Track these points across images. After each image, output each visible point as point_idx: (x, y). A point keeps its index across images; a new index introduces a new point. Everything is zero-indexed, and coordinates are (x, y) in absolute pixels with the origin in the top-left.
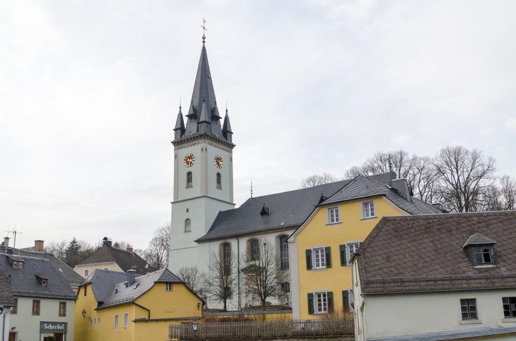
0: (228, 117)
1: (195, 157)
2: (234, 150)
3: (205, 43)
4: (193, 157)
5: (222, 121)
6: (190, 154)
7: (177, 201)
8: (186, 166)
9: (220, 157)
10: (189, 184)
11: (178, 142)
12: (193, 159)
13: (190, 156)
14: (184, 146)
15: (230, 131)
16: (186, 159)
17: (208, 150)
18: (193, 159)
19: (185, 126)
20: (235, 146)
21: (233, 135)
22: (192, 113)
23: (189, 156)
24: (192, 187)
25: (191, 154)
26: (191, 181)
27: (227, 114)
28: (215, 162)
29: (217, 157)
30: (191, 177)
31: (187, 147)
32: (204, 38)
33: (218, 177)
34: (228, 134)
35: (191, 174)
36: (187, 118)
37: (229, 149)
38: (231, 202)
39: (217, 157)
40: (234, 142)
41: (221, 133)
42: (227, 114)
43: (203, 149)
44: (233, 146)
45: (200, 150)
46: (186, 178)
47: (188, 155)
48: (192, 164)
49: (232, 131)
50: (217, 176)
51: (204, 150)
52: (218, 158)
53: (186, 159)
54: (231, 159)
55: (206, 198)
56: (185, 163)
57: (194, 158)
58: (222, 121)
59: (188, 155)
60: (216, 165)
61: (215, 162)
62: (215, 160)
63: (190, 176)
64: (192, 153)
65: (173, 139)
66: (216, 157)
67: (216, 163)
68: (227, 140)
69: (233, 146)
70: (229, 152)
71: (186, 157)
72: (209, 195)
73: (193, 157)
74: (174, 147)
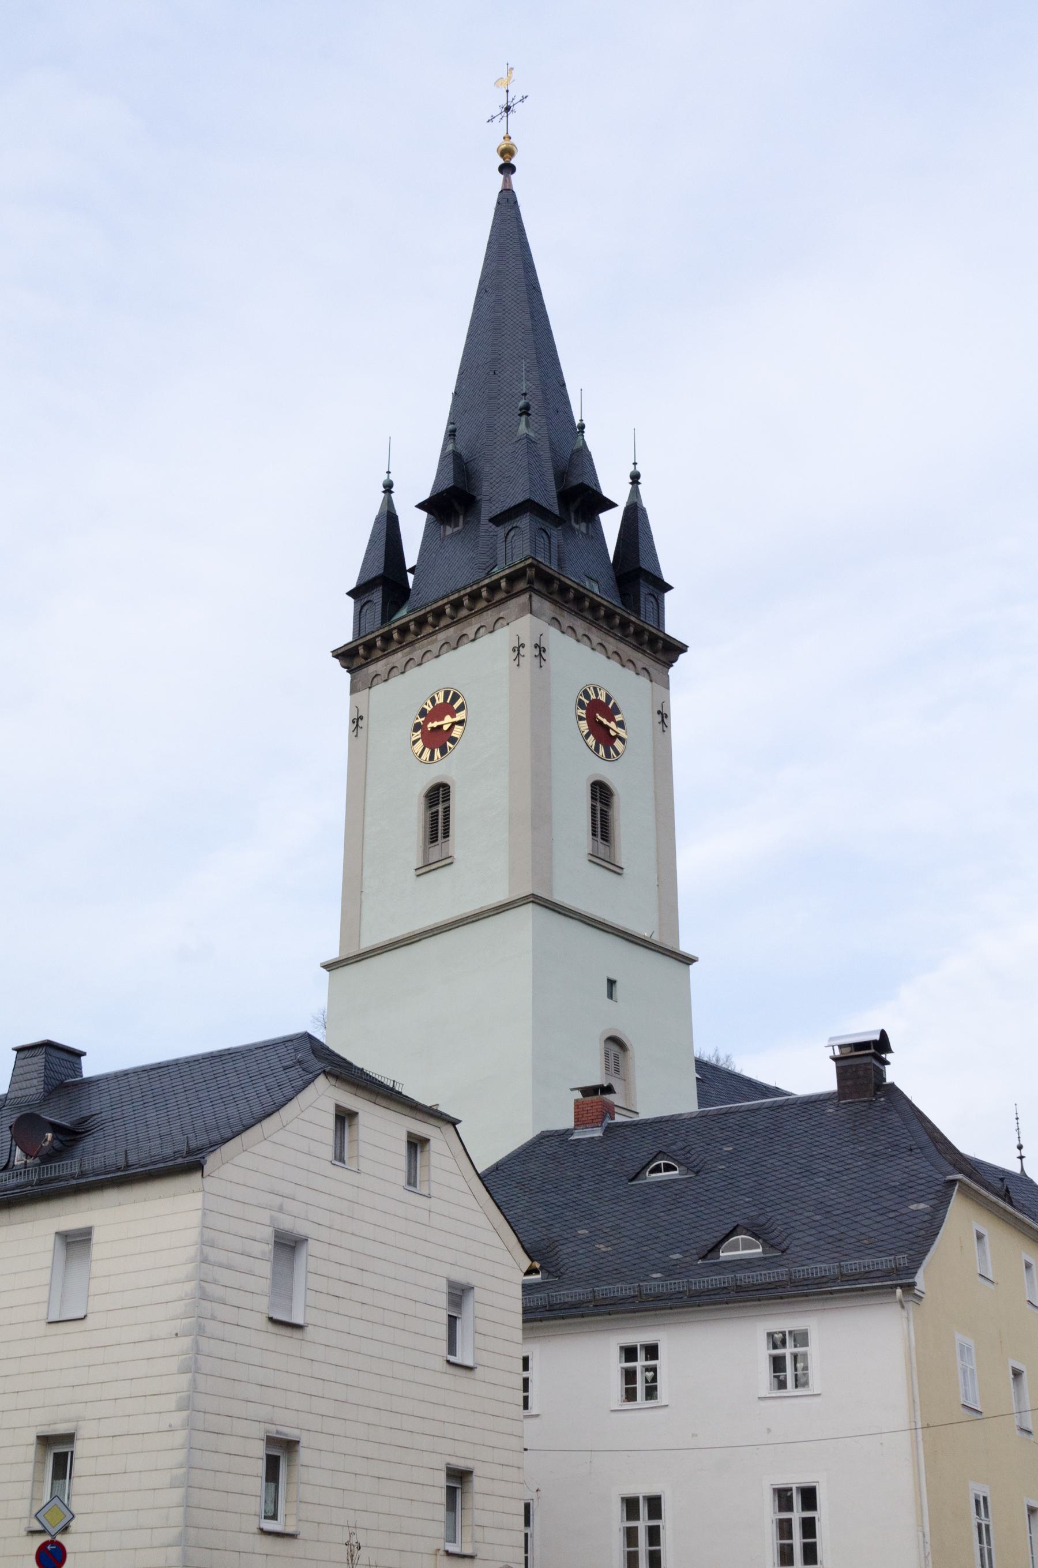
0: (644, 510)
1: (469, 705)
2: (680, 669)
3: (513, 177)
4: (456, 706)
5: (610, 523)
6: (442, 694)
7: (353, 951)
8: (424, 757)
9: (609, 698)
10: (435, 853)
11: (370, 646)
12: (460, 716)
13: (441, 701)
14: (400, 664)
15: (656, 574)
16: (421, 720)
17: (550, 655)
18: (460, 716)
19: (411, 558)
20: (682, 648)
21: (668, 596)
22: (448, 483)
23: (438, 702)
24: (447, 861)
25: (447, 694)
26: (446, 834)
27: (635, 493)
28: (581, 718)
29: (593, 697)
30: (447, 810)
31: (420, 664)
32: (507, 152)
33: (599, 806)
34: (644, 590)
35: (447, 798)
36: (423, 515)
37: (654, 667)
38: (669, 945)
39: (593, 697)
40: (673, 627)
41: (608, 579)
42: (635, 493)
43: (523, 646)
44: (672, 650)
45: (508, 655)
46: (422, 817)
47: (433, 700)
48: (454, 740)
49: (667, 579)
50: (593, 798)
51: (528, 651)
52: (597, 702)
53: (421, 720)
54: (663, 716)
55: (534, 905)
56: (415, 742)
57: (462, 707)
58: (610, 523)
59: (433, 700)
60: (587, 736)
61: (581, 718)
62: (582, 713)
63: (440, 808)
64: (456, 686)
65: (345, 635)
66: (586, 694)
67: (584, 725)
68: (637, 612)
69: (672, 650)
70: (651, 681)
71: (423, 713)
72: (559, 897)
73: (456, 706)
74: (347, 677)
